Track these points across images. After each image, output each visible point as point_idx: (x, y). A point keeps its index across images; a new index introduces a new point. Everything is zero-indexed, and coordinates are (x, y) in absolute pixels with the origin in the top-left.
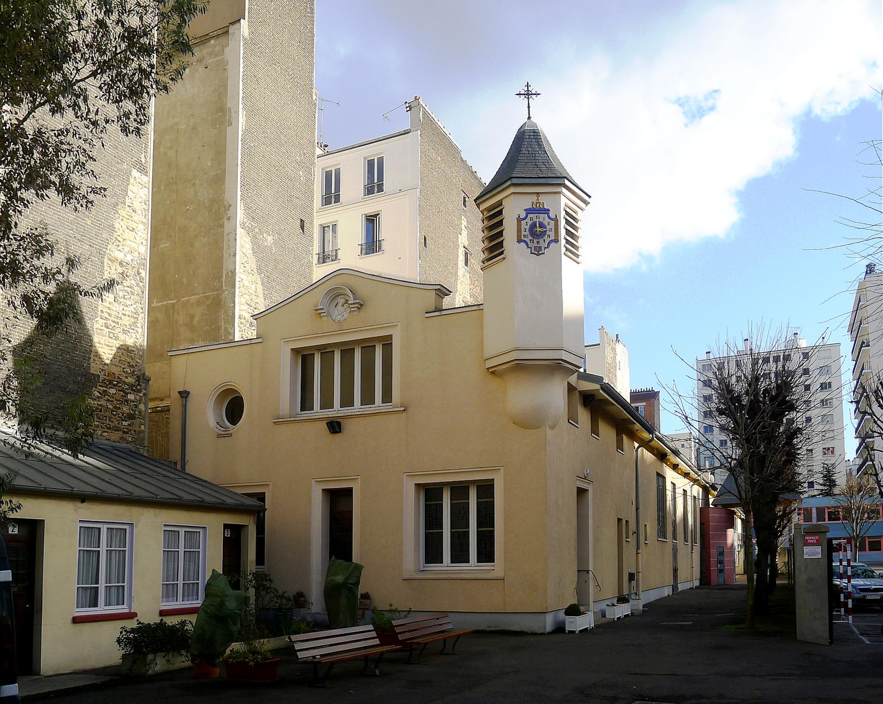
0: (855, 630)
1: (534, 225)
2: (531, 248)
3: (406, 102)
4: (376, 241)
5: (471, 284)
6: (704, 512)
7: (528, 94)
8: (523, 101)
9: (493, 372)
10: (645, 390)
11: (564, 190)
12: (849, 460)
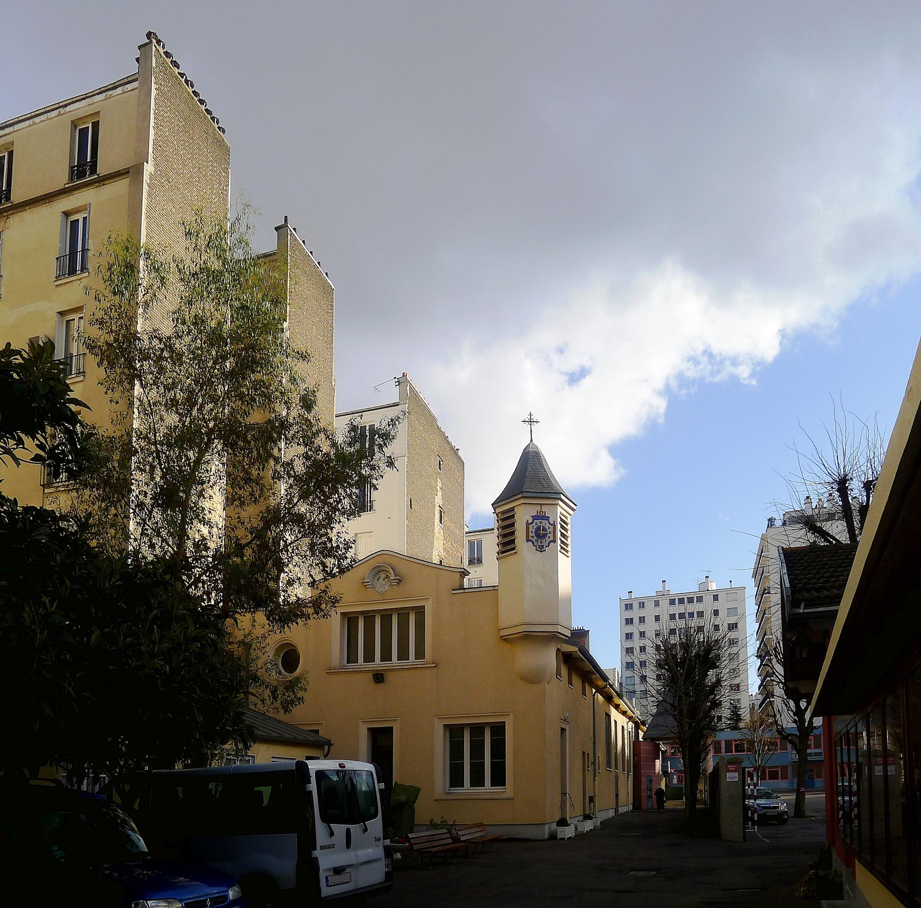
0: (760, 835)
1: (538, 529)
2: (536, 546)
3: (395, 378)
4: (367, 501)
5: (444, 540)
6: (636, 744)
7: (531, 422)
8: (527, 426)
9: (505, 639)
10: (577, 629)
11: (560, 503)
12: (752, 695)
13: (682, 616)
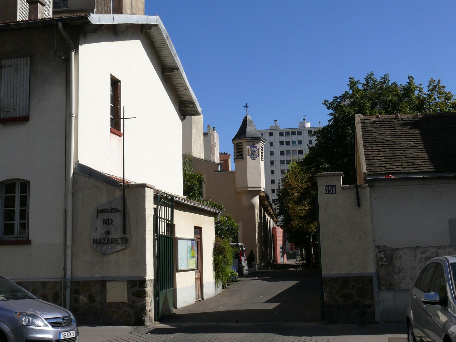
1: (252, 151)
7: (247, 107)
8: (245, 109)
10: (222, 153)
13: (288, 143)
